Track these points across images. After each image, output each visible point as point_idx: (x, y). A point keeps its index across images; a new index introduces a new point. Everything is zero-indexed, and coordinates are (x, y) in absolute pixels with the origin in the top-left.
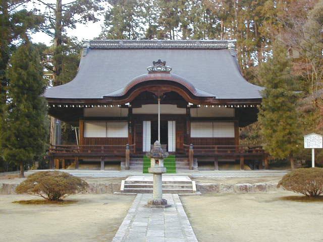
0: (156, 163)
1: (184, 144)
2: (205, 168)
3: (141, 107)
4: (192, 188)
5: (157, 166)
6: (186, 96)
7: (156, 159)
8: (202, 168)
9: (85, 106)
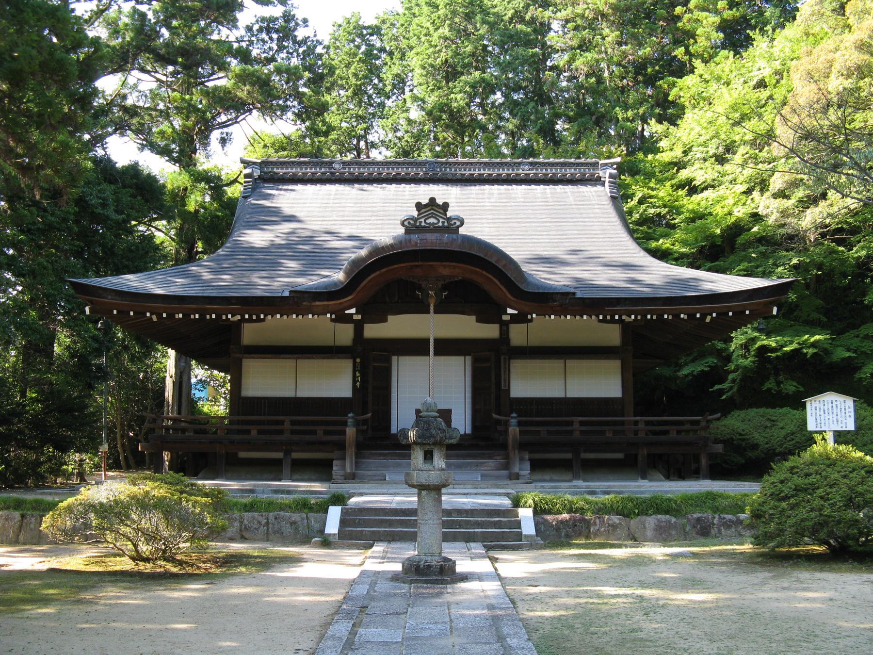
0: (425, 459)
1: (494, 415)
2: (843, 567)
3: (386, 320)
4: (520, 528)
5: (427, 466)
6: (501, 292)
7: (427, 448)
8: (538, 476)
9: (243, 317)
